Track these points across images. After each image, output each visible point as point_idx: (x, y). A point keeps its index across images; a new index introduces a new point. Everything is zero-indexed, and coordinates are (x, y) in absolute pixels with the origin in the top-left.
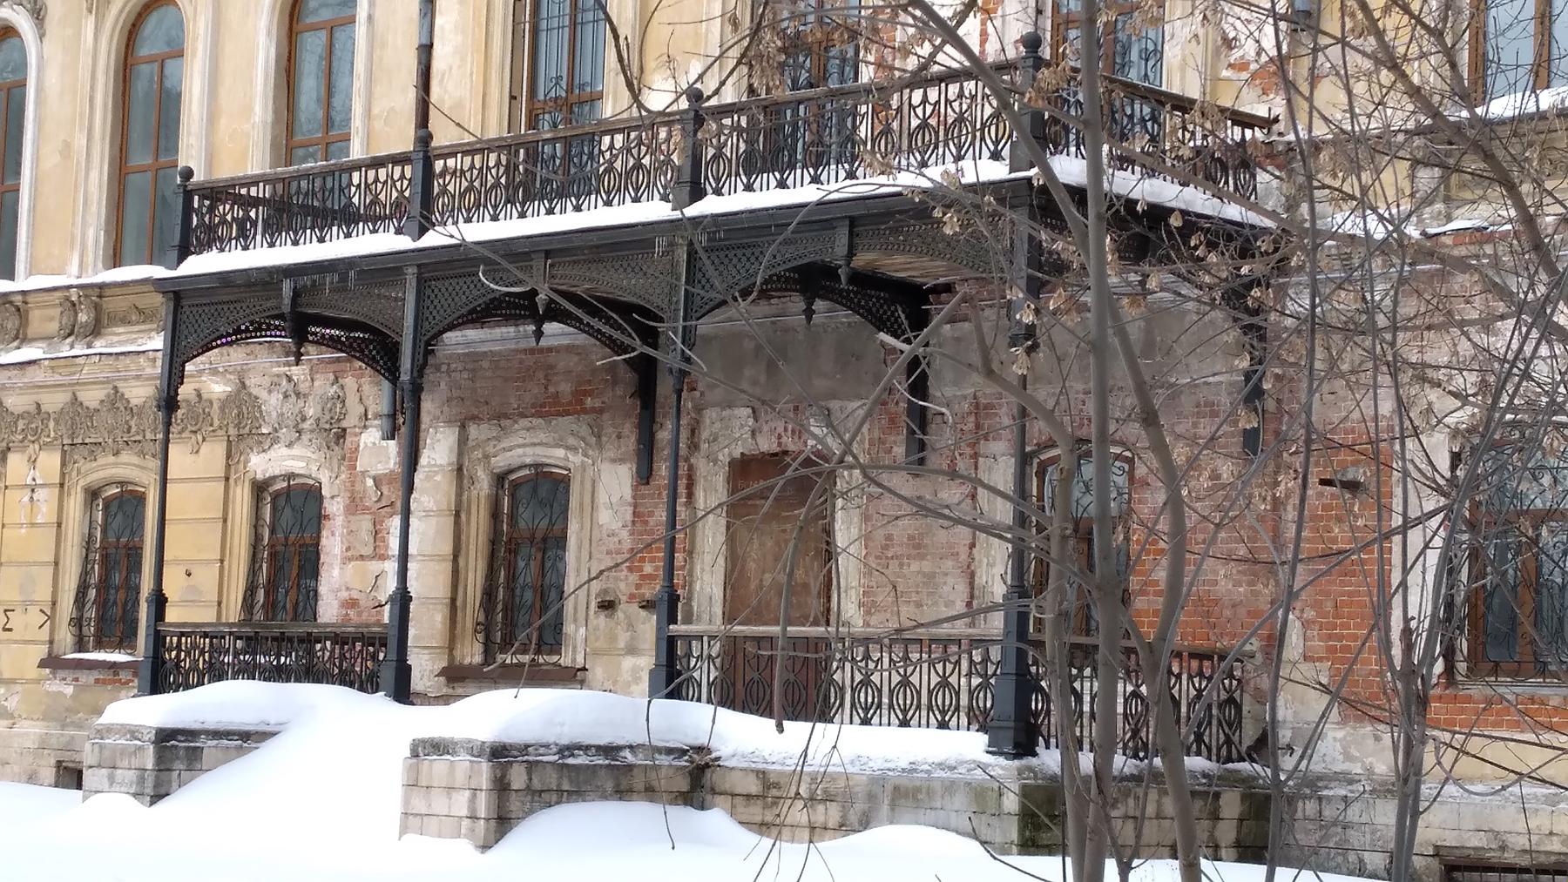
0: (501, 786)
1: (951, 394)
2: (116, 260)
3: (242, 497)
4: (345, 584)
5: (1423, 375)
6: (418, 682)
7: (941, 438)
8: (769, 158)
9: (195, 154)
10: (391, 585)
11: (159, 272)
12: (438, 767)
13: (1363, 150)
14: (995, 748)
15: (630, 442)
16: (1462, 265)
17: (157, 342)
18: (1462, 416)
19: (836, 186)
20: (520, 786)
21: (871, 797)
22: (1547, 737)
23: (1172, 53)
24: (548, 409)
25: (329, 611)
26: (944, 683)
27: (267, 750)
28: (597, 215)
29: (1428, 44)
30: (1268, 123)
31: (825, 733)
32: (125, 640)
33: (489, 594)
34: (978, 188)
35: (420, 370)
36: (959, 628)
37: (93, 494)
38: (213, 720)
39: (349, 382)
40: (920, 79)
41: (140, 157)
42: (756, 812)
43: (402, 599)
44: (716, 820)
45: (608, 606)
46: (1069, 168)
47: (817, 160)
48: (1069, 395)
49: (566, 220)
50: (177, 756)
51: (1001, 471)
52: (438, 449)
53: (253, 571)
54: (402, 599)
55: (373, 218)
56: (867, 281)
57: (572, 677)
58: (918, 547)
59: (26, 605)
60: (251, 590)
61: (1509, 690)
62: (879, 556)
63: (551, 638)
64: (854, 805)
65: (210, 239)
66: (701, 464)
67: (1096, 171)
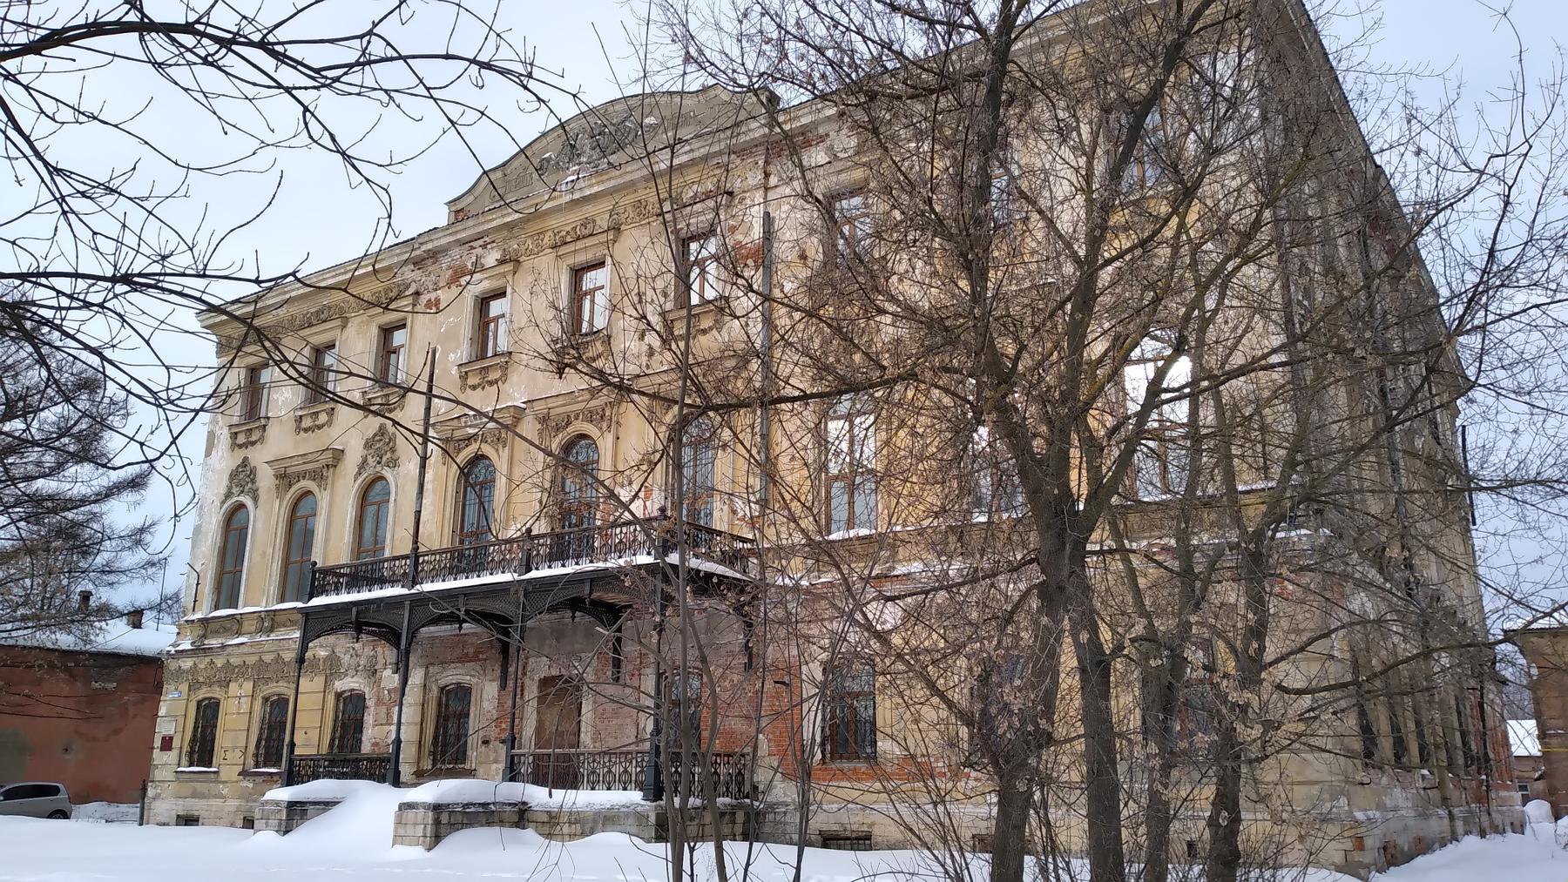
0: (437, 822)
1: (630, 648)
2: (282, 600)
3: (331, 699)
4: (374, 736)
5: (807, 638)
6: (403, 778)
7: (626, 667)
8: (559, 554)
9: (318, 556)
10: (393, 736)
11: (300, 605)
12: (411, 814)
13: (782, 552)
14: (645, 798)
15: (498, 673)
16: (822, 597)
17: (297, 634)
18: (824, 656)
19: (586, 566)
20: (445, 822)
21: (595, 821)
22: (859, 786)
23: (716, 514)
24: (463, 659)
25: (366, 748)
26: (626, 771)
27: (336, 810)
28: (487, 579)
29: (807, 512)
30: (751, 541)
31: (571, 793)
32: (277, 764)
33: (435, 738)
34: (640, 567)
35: (409, 644)
36: (633, 748)
37: (266, 699)
38: (312, 797)
39: (379, 649)
40: (614, 525)
41: (295, 557)
42: (546, 829)
43: (398, 742)
44: (530, 833)
45: (486, 742)
46: (674, 558)
47: (578, 557)
48: (673, 650)
49: (474, 581)
50: (296, 813)
51: (649, 684)
52: (416, 677)
53: (334, 731)
54: (398, 742)
55: (392, 582)
56: (597, 604)
57: (470, 774)
58: (616, 714)
59: (234, 748)
60: (333, 740)
61: (846, 765)
62: (600, 716)
63: (461, 756)
64: (588, 824)
65: (323, 591)
66: (527, 682)
67: (683, 559)
